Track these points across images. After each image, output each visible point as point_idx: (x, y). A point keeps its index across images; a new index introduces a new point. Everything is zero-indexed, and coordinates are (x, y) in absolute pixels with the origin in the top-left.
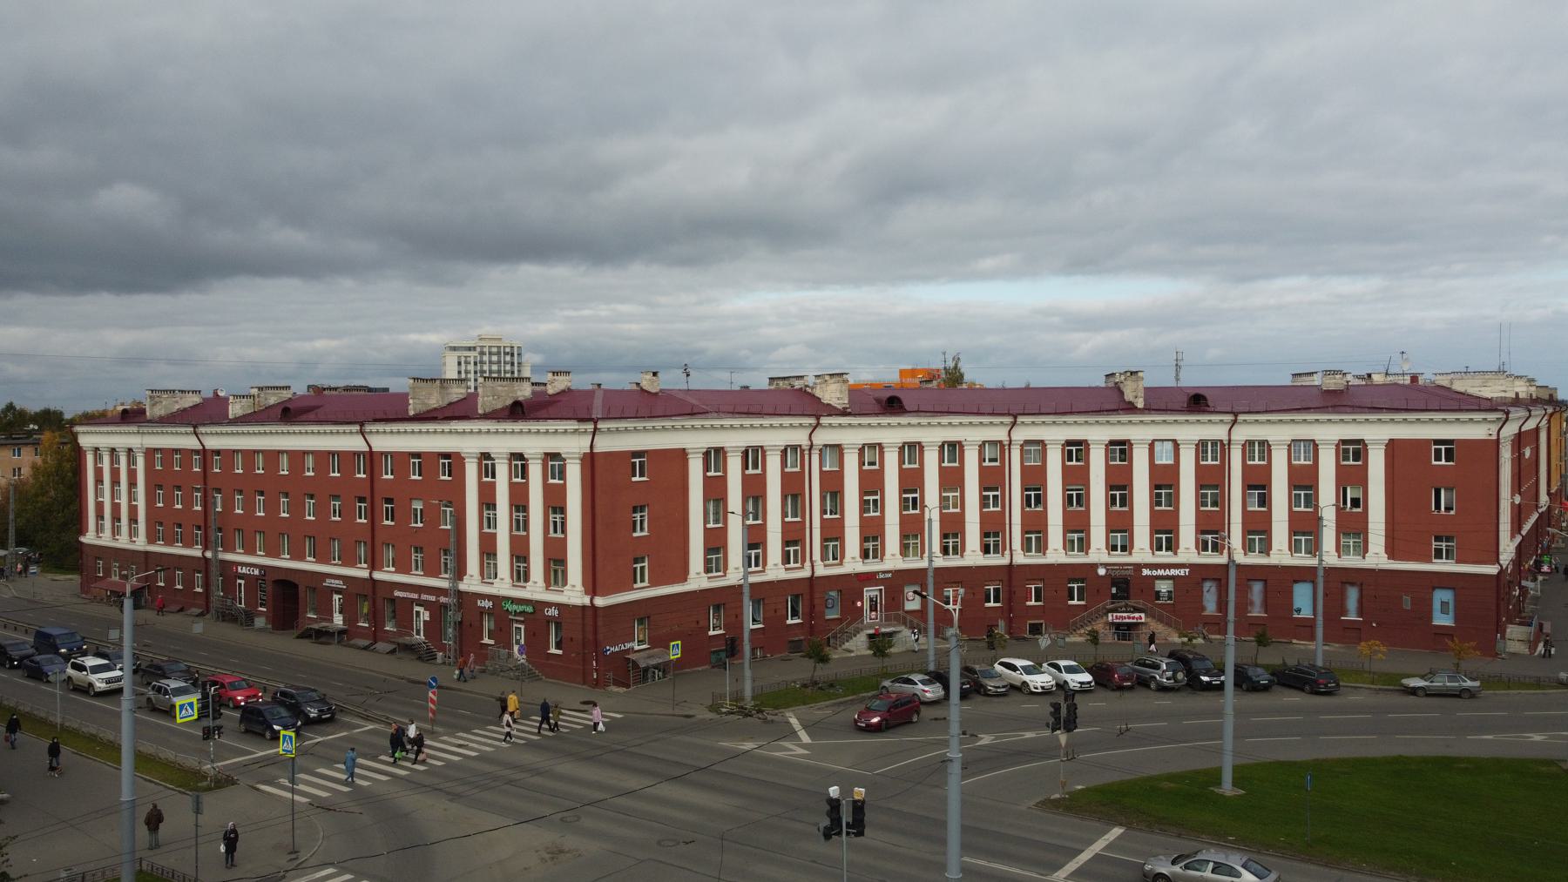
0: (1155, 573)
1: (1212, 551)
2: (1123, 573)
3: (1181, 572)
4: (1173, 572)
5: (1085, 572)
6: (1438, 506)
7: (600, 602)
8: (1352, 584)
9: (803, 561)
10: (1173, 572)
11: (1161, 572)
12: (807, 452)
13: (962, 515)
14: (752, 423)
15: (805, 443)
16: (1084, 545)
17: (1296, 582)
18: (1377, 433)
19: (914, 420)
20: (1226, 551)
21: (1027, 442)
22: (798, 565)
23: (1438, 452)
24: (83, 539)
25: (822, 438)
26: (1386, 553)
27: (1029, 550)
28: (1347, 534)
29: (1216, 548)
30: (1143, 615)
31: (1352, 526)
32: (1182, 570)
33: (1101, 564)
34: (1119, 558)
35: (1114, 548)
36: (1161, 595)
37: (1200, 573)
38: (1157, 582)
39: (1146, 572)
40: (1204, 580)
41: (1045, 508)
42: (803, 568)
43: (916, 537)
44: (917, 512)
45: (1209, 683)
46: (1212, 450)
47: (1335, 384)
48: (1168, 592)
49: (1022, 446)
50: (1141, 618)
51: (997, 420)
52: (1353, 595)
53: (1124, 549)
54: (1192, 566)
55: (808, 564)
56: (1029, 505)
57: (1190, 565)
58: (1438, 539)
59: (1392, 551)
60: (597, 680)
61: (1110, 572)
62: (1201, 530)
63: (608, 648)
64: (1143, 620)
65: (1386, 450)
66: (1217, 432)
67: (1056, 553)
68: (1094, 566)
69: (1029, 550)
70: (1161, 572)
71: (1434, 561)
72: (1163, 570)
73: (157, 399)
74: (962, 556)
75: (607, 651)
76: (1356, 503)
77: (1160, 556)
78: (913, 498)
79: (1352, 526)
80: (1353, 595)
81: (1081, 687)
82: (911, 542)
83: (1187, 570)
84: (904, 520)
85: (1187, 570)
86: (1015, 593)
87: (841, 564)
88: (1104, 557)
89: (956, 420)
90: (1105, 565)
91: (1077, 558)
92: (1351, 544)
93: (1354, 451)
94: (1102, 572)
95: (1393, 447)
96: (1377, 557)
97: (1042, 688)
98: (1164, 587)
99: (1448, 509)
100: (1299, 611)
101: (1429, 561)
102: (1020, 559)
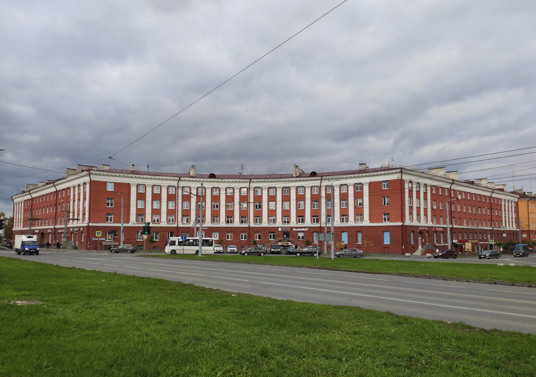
0: (297, 230)
1: (316, 223)
2: (287, 230)
3: (306, 230)
4: (303, 229)
5: (273, 231)
6: (385, 204)
7: (90, 224)
8: (359, 232)
9: (175, 222)
10: (303, 229)
11: (299, 230)
12: (177, 188)
13: (233, 211)
14: (147, 177)
15: (176, 185)
16: (275, 221)
17: (342, 232)
18: (366, 180)
19: (220, 180)
20: (320, 223)
21: (255, 188)
22: (174, 223)
23: (384, 185)
24: (13, 230)
25: (182, 184)
26: (369, 220)
27: (257, 222)
28: (358, 215)
29: (317, 221)
30: (290, 243)
31: (359, 212)
32: (306, 229)
33: (280, 227)
34: (286, 225)
35: (285, 222)
36: (300, 237)
37: (312, 230)
38: (298, 233)
39: (294, 230)
40: (313, 232)
41: (262, 209)
42: (175, 224)
43: (217, 217)
44: (218, 209)
45: (273, 251)
46: (316, 189)
47: (363, 168)
48: (303, 236)
49: (254, 189)
50: (289, 244)
51: (245, 180)
52: (360, 235)
53: (288, 222)
54: (309, 228)
55: (176, 223)
56: (257, 208)
57: (309, 227)
58: (385, 215)
59: (371, 220)
60: (89, 248)
61: (283, 229)
62: (313, 216)
63: (93, 238)
64: (290, 244)
65: (369, 186)
66: (317, 183)
67: (265, 223)
68: (278, 228)
69: (257, 222)
70: (299, 230)
71: (384, 222)
72: (301, 229)
73: (29, 187)
74: (233, 224)
75: (92, 239)
76: (361, 204)
77: (299, 224)
78: (216, 205)
79: (359, 212)
80: (360, 235)
81: (230, 251)
82: (216, 219)
83: (308, 229)
84: (212, 212)
85: (308, 229)
86: (251, 236)
87: (189, 224)
88: (281, 225)
89: (231, 180)
90: (281, 227)
91: (272, 225)
92: (359, 218)
93: (358, 188)
94: (280, 230)
95: (371, 184)
96: (366, 222)
97: (217, 251)
98: (301, 235)
99: (387, 204)
100: (344, 242)
101: (382, 222)
102: (252, 225)
